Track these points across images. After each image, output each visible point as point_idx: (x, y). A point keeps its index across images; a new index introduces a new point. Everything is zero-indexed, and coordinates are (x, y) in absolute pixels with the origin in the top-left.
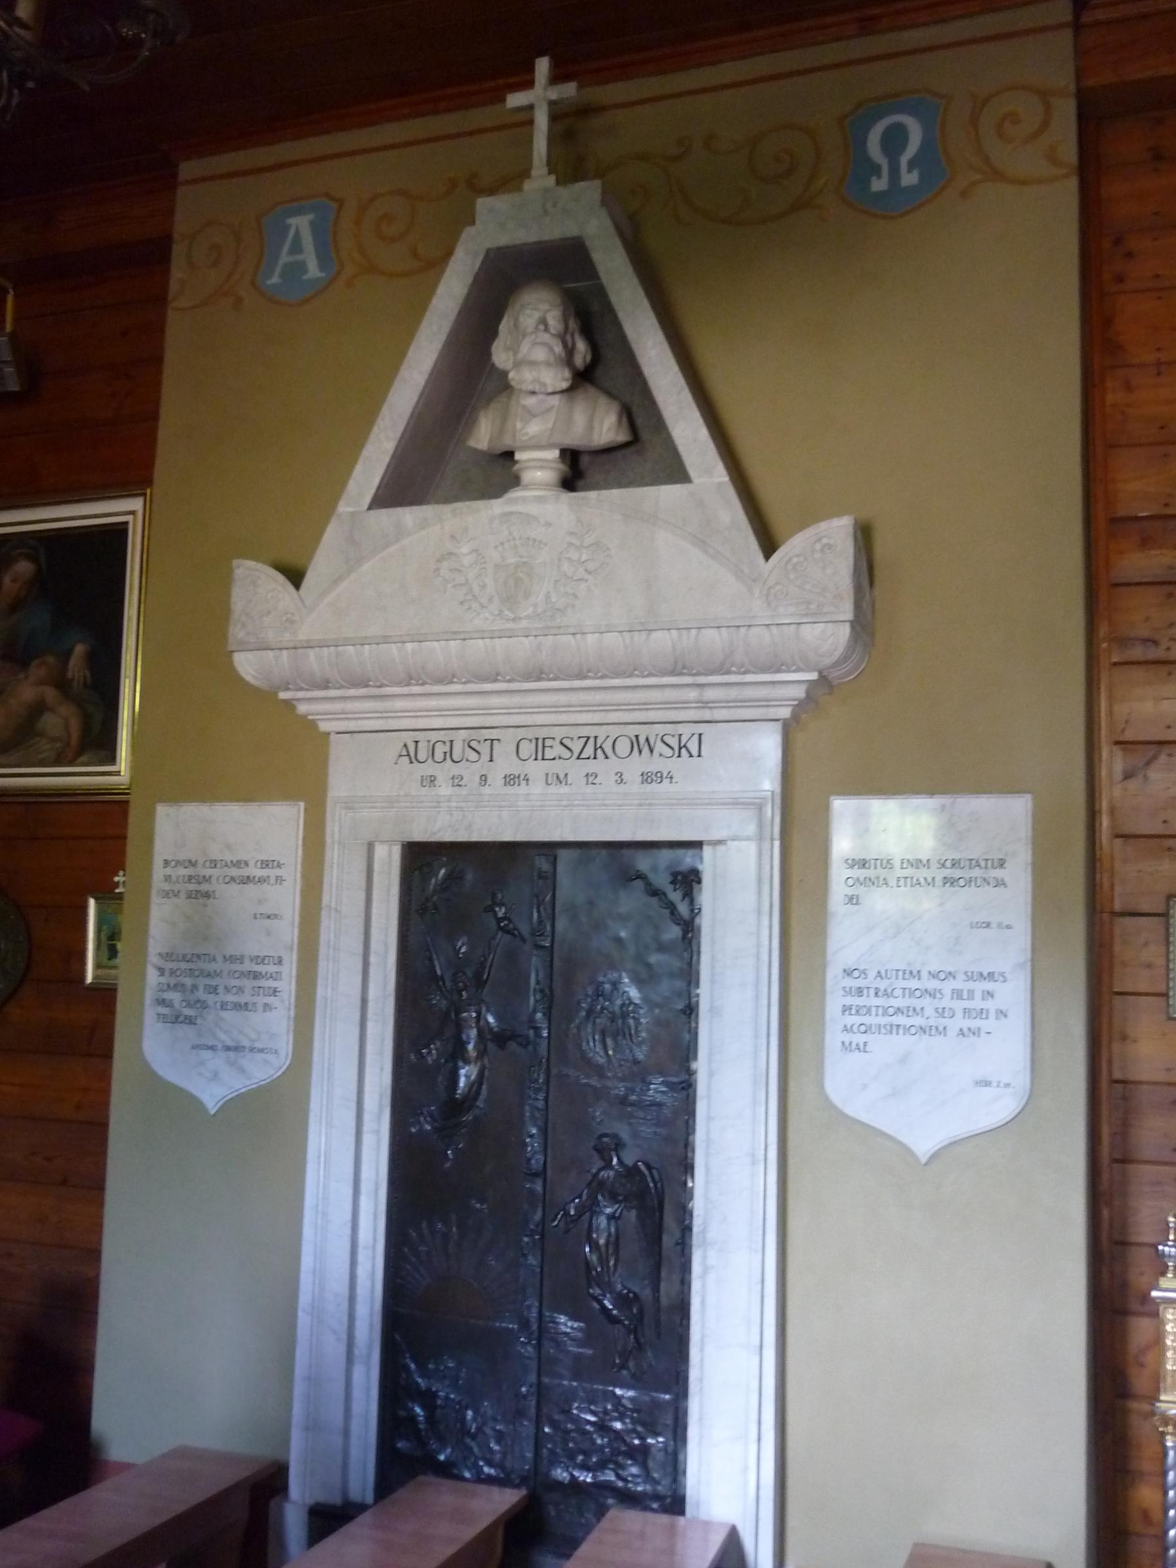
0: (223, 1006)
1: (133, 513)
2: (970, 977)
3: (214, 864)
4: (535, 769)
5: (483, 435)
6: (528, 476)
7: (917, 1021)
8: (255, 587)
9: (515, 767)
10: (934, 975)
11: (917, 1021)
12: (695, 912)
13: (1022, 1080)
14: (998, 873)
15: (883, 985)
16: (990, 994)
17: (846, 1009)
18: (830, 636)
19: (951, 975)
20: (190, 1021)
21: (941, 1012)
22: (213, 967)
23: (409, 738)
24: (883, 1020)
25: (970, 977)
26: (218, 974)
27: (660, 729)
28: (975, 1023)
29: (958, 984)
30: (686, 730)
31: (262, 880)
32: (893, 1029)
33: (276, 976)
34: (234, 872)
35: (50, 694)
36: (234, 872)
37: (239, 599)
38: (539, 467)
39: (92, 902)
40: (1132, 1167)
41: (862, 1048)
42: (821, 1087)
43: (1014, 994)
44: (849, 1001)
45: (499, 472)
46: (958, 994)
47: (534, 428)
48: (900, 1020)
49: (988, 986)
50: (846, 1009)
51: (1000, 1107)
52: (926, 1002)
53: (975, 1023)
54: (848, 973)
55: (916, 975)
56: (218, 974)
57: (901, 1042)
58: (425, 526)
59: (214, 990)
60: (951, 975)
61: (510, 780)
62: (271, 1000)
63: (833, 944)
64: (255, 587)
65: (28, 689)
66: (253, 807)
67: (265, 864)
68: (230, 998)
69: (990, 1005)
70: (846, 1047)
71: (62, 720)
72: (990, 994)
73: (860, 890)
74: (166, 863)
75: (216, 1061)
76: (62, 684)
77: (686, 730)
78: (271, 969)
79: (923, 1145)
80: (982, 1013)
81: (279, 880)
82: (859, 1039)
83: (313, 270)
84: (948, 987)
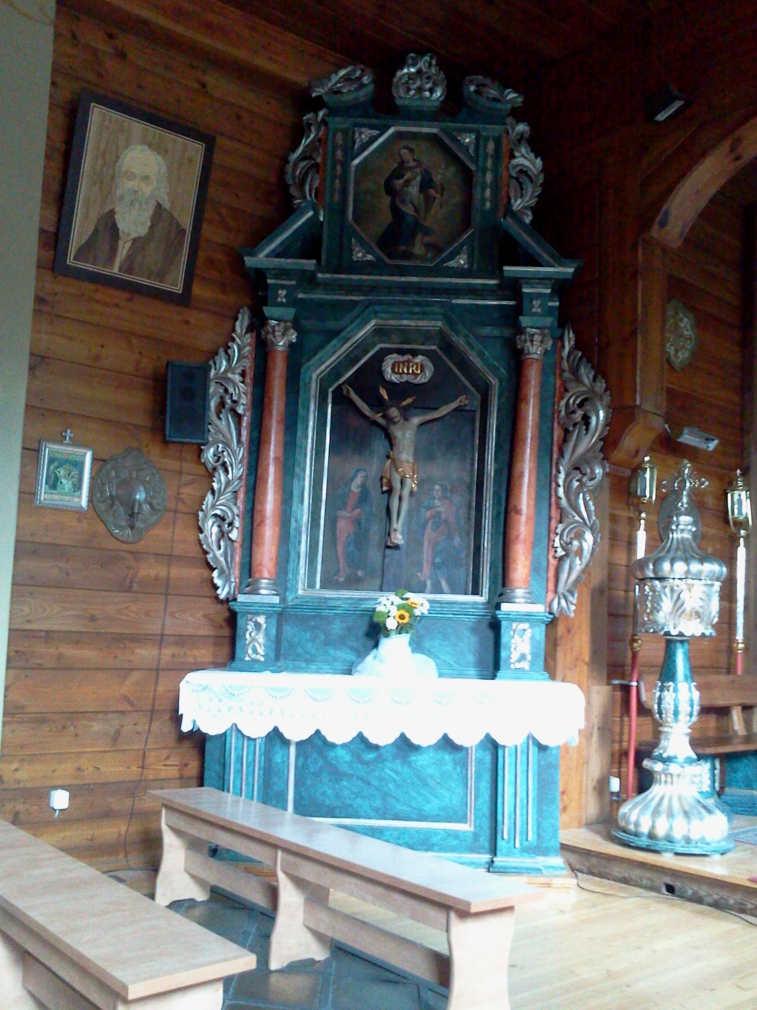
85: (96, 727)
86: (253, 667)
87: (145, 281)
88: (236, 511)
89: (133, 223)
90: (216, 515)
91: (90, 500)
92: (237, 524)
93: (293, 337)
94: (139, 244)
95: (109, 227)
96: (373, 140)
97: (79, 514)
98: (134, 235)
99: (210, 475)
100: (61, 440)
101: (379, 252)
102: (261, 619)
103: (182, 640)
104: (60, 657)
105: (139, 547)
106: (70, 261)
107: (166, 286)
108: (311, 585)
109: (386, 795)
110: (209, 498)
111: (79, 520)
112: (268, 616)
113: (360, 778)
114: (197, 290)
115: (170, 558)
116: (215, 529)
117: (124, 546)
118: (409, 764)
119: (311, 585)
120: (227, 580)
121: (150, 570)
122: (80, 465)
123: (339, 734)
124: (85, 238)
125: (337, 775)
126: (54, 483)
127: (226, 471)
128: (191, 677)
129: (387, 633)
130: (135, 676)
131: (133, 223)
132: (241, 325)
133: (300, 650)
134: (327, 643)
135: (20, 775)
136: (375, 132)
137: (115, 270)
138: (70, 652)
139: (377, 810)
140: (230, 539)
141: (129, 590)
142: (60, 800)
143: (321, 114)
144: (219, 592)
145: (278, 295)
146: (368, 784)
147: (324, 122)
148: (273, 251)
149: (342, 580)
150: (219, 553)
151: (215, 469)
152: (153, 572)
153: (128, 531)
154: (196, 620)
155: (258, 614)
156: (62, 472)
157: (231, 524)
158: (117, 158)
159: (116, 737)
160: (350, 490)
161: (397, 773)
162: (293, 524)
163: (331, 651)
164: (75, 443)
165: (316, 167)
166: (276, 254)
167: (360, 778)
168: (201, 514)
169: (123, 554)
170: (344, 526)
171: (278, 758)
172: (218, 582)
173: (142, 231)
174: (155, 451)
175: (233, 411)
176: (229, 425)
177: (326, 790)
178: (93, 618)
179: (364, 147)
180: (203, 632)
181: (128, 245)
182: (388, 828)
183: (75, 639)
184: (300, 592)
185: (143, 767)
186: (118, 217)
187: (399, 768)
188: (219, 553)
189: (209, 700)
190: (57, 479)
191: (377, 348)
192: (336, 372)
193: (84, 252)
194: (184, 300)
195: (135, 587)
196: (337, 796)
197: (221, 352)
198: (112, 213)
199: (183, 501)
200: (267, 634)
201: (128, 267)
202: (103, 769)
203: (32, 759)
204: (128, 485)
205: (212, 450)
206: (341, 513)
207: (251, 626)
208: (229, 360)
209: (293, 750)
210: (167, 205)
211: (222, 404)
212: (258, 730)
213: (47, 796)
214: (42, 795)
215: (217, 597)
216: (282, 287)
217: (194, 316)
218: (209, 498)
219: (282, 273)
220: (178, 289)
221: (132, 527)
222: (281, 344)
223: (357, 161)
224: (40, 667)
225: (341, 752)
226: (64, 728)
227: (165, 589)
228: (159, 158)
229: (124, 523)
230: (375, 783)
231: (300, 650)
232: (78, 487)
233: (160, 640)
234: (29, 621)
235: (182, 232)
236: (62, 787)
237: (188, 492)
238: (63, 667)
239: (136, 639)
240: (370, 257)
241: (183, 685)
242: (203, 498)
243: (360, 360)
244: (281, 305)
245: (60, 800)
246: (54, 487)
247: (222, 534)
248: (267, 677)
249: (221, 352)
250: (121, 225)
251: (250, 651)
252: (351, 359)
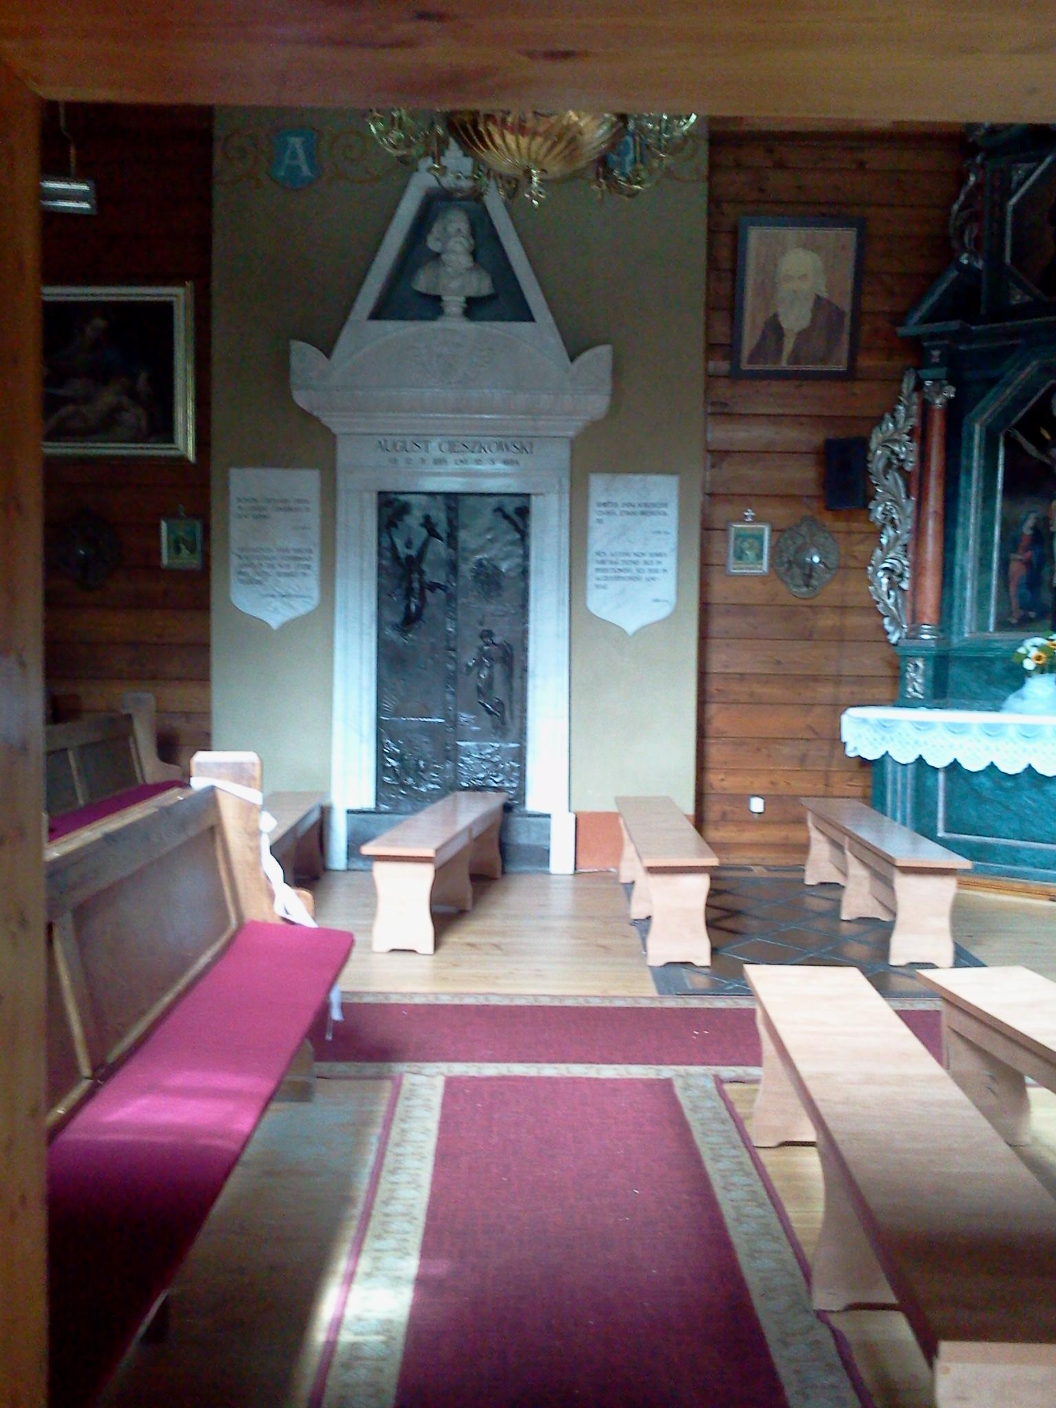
0: (279, 574)
1: (176, 296)
2: (651, 555)
3: (269, 501)
4: (451, 458)
5: (423, 282)
6: (447, 310)
7: (628, 574)
8: (303, 354)
9: (438, 454)
10: (636, 554)
11: (628, 574)
12: (526, 526)
13: (672, 598)
14: (664, 509)
15: (613, 559)
16: (659, 562)
17: (598, 570)
18: (598, 404)
19: (643, 554)
20: (259, 582)
21: (638, 571)
22: (270, 555)
23: (381, 439)
24: (613, 574)
25: (651, 555)
26: (274, 558)
27: (461, 439)
28: (652, 575)
29: (647, 558)
30: (524, 440)
31: (297, 510)
32: (618, 578)
33: (309, 559)
34: (281, 505)
35: (125, 400)
36: (281, 505)
37: (294, 361)
38: (454, 303)
39: (164, 526)
40: (711, 568)
41: (604, 587)
42: (585, 605)
43: (670, 562)
44: (599, 566)
45: (432, 306)
46: (646, 563)
47: (454, 284)
48: (622, 574)
49: (659, 559)
50: (598, 570)
51: (664, 611)
52: (633, 567)
53: (652, 575)
54: (598, 554)
55: (627, 554)
56: (274, 558)
57: (622, 583)
58: (395, 330)
59: (272, 566)
60: (643, 554)
61: (438, 462)
62: (307, 571)
63: (590, 541)
64: (303, 354)
65: (108, 397)
66: (289, 471)
67: (299, 501)
68: (284, 570)
69: (660, 567)
70: (597, 586)
71: (133, 416)
72: (659, 562)
73: (604, 517)
74: (239, 500)
75: (276, 603)
76: (133, 394)
77: (524, 440)
78: (307, 555)
79: (630, 628)
80: (656, 571)
81: (308, 509)
82: (602, 583)
83: (305, 170)
84: (641, 559)
85: (786, 750)
86: (911, 704)
87: (811, 367)
88: (905, 563)
89: (795, 319)
90: (885, 569)
91: (771, 566)
92: (907, 575)
93: (950, 392)
94: (803, 336)
95: (774, 328)
96: (1029, 173)
97: (762, 578)
98: (797, 330)
99: (879, 533)
100: (742, 520)
101: (1038, 291)
102: (920, 664)
103: (860, 679)
104: (752, 694)
105: (816, 601)
106: (745, 366)
107: (832, 367)
108: (983, 627)
109: (1022, 819)
110: (878, 552)
111: (764, 584)
112: (926, 659)
113: (1000, 803)
114: (864, 362)
115: (843, 609)
116: (885, 581)
117: (803, 602)
118: (1044, 793)
119: (983, 627)
120: (898, 626)
121: (827, 621)
122: (760, 538)
123: (973, 764)
124: (755, 342)
125: (980, 799)
126: (740, 556)
127: (895, 527)
128: (852, 712)
129: (1028, 674)
130: (818, 710)
131: (795, 319)
132: (908, 384)
133: (964, 689)
134: (990, 682)
135: (725, 784)
136: (1031, 165)
137: (784, 364)
138: (759, 689)
139: (1014, 831)
140: (901, 588)
141: (809, 638)
142: (757, 805)
143: (979, 159)
144: (889, 637)
145: (932, 356)
146: (1007, 808)
147: (983, 166)
148: (921, 318)
149: (1014, 621)
150: (890, 602)
151: (884, 526)
152: (830, 623)
153: (804, 589)
154: (870, 662)
155: (916, 657)
156: (746, 545)
157: (901, 576)
158: (776, 265)
159: (803, 759)
160: (1022, 534)
161: (1034, 801)
162: (958, 571)
163: (993, 689)
164: (756, 520)
165: (976, 217)
166: (925, 320)
167: (1000, 803)
168: (870, 568)
169: (805, 609)
170: (1017, 569)
171: (929, 783)
172: (889, 628)
173: (805, 322)
174: (828, 519)
175: (901, 470)
176: (896, 482)
177: (971, 813)
178: (779, 663)
179: (1020, 184)
180: (881, 673)
181: (792, 340)
182: (1024, 848)
183: (765, 679)
184: (966, 635)
185: (827, 785)
186: (781, 319)
187: (1036, 797)
188: (890, 602)
189: (866, 731)
190: (742, 551)
191: (1048, 385)
192: (1005, 414)
193: (753, 359)
194: (850, 375)
195: (816, 636)
196: (980, 818)
197: (887, 416)
198: (776, 316)
199: (855, 557)
200: (924, 675)
201: (795, 358)
202: (792, 783)
203: (734, 772)
204: (802, 549)
205: (880, 509)
206: (1013, 556)
207: (911, 668)
208: (895, 423)
209: (941, 776)
210: (824, 295)
211: (889, 464)
212: (909, 758)
213: (748, 803)
214: (744, 799)
215: (888, 641)
216: (935, 348)
217: (859, 388)
218: (878, 552)
219: (932, 336)
220: (842, 367)
221: (807, 586)
222: (938, 401)
223: (1014, 200)
224: (737, 702)
225: (983, 780)
226: (759, 750)
227: (840, 637)
228: (815, 255)
229: (801, 582)
230: (1013, 807)
231: (964, 689)
232: (759, 556)
233: (838, 679)
234: (726, 666)
235: (841, 314)
236: (758, 796)
237: (860, 549)
238: (756, 702)
239: (815, 679)
240: (1028, 298)
241: (845, 718)
242: (872, 552)
243: (1029, 400)
244: (936, 365)
245: (757, 805)
246: (740, 558)
247: (892, 585)
248: (922, 714)
249: (887, 416)
250: (784, 326)
251: (910, 690)
252: (1018, 402)
